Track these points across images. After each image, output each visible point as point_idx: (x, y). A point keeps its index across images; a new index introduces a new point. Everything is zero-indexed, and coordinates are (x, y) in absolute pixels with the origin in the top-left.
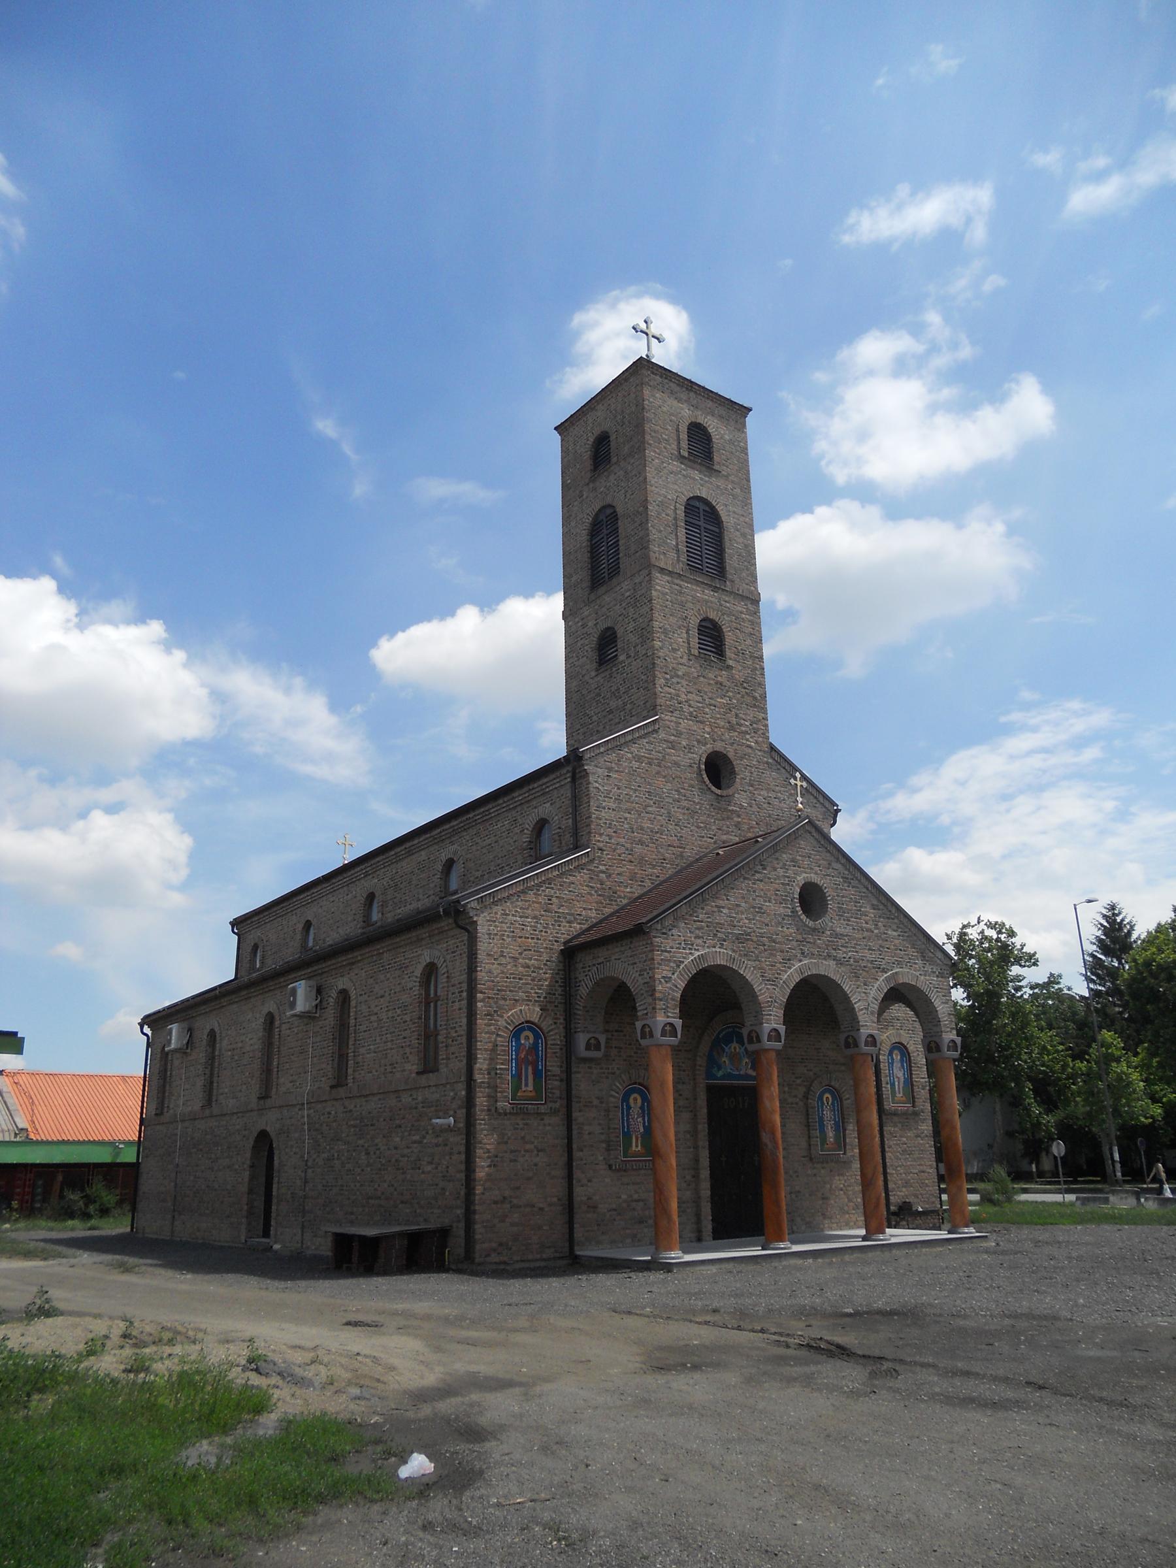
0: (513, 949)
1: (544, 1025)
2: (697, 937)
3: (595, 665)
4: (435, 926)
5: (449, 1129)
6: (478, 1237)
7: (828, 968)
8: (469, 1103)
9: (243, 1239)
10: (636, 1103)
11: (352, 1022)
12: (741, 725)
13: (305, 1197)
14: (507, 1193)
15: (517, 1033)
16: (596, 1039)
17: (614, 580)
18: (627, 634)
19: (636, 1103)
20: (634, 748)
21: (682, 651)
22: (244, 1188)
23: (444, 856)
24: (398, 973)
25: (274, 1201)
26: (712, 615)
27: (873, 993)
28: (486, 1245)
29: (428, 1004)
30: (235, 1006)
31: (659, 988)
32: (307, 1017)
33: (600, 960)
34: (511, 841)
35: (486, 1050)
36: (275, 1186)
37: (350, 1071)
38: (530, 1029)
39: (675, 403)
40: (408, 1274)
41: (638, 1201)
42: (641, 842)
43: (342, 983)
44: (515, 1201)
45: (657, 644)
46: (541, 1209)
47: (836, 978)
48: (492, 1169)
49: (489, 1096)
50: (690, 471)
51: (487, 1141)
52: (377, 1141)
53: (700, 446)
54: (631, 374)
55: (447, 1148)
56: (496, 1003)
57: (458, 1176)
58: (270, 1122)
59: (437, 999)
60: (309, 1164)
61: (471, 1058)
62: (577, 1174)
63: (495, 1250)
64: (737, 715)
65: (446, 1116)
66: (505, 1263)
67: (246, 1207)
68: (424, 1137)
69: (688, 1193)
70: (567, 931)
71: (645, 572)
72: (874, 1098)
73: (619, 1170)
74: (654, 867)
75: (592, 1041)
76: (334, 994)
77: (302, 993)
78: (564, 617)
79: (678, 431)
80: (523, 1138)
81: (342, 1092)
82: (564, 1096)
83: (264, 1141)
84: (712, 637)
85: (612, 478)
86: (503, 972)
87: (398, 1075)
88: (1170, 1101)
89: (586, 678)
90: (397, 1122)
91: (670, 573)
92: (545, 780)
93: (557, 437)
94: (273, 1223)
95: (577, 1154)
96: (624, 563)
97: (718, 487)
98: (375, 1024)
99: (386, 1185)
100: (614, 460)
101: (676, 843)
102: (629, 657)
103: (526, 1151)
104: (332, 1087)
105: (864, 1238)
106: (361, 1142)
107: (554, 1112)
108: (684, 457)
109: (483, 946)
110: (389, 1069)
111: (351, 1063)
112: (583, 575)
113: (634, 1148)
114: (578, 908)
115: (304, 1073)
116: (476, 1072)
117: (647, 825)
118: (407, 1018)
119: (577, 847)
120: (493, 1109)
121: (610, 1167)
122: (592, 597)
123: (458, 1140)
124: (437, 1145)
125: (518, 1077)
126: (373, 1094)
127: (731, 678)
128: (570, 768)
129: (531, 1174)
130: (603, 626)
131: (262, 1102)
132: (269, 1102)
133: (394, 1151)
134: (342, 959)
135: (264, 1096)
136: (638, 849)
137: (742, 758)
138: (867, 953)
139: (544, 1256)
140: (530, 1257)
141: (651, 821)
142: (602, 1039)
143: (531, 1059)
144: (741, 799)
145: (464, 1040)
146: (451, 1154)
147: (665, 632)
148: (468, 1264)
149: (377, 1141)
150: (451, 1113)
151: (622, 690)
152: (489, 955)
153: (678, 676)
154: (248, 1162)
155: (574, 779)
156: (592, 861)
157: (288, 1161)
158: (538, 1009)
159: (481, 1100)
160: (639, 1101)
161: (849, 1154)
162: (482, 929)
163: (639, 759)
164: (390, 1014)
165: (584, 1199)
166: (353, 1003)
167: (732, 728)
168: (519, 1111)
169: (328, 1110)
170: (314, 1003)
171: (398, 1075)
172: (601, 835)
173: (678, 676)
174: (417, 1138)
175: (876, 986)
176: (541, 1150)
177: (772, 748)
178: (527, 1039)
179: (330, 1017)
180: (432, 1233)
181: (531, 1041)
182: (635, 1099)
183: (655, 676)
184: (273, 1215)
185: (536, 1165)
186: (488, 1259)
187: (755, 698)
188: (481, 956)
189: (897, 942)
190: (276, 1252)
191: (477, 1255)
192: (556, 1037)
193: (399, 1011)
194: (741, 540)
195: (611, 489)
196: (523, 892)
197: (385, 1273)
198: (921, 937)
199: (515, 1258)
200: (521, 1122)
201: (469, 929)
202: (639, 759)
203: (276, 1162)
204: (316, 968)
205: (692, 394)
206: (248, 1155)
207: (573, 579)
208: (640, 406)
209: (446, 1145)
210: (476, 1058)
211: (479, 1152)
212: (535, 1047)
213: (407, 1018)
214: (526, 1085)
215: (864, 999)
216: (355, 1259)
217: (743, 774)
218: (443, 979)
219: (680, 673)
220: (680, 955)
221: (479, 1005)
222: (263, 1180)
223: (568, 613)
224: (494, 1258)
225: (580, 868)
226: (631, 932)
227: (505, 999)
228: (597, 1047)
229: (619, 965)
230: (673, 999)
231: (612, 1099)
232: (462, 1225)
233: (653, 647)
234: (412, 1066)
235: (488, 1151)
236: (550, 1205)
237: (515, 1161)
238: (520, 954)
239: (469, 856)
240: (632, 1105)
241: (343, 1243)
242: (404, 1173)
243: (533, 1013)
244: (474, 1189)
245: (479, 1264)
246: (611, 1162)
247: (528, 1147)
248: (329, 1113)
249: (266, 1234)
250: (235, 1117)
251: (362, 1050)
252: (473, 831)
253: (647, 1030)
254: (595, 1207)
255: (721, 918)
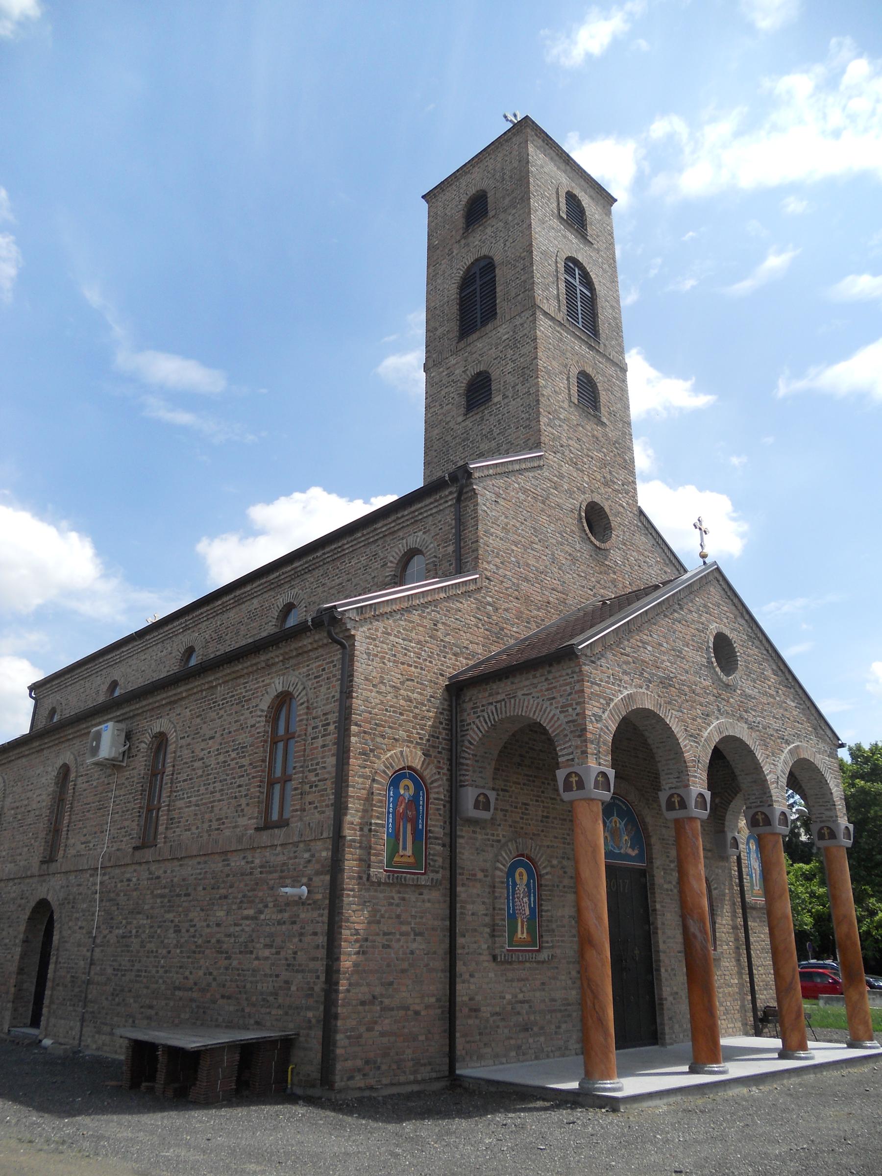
0: (395, 676)
1: (427, 774)
2: (625, 673)
3: (462, 410)
4: (294, 645)
5: (300, 902)
6: (339, 1051)
7: (741, 731)
8: (335, 866)
9: (6, 1028)
10: (521, 879)
11: (169, 770)
12: (614, 483)
13: (89, 982)
14: (378, 990)
15: (395, 782)
16: (486, 796)
17: (490, 326)
18: (503, 376)
19: (521, 879)
20: (521, 479)
21: (564, 396)
22: (13, 967)
23: (281, 600)
24: (236, 708)
25: (49, 984)
26: (589, 370)
27: (780, 766)
28: (349, 1064)
29: (274, 743)
30: (24, 760)
31: (590, 727)
32: (113, 766)
33: (499, 697)
34: (369, 578)
35: (359, 798)
36: (51, 967)
37: (161, 829)
38: (411, 778)
39: (555, 169)
40: (239, 1104)
41: (522, 1002)
42: (526, 580)
43: (159, 725)
44: (387, 1001)
45: (542, 382)
46: (417, 1013)
47: (749, 742)
48: (361, 958)
49: (360, 860)
50: (568, 234)
51: (356, 918)
52: (191, 915)
53: (575, 217)
54: (514, 135)
55: (296, 927)
56: (373, 740)
57: (312, 965)
58: (52, 890)
59: (290, 736)
60: (98, 941)
61: (340, 808)
62: (460, 967)
63: (359, 1070)
64: (610, 472)
65: (296, 883)
66: (371, 1088)
67: (12, 990)
68: (261, 912)
69: (574, 992)
70: (457, 665)
71: (527, 314)
72: (705, 891)
73: (502, 963)
74: (539, 609)
75: (481, 798)
76: (147, 738)
77: (108, 738)
78: (426, 369)
79: (557, 193)
80: (398, 917)
81: (148, 854)
82: (448, 866)
83: (43, 915)
84: (588, 394)
85: (489, 231)
86: (382, 703)
87: (227, 832)
88: (817, 911)
89: (451, 425)
90: (223, 892)
91: (552, 319)
92: (420, 505)
93: (425, 205)
94: (45, 1011)
95: (460, 941)
96: (502, 306)
97: (591, 257)
98: (200, 772)
99: (201, 973)
100: (491, 214)
101: (560, 588)
102: (505, 397)
103: (402, 934)
104: (136, 848)
105: (784, 1054)
106: (170, 916)
107: (435, 885)
108: (562, 218)
109: (361, 667)
110: (215, 825)
111: (163, 819)
112: (453, 326)
113: (519, 935)
114: (465, 638)
115: (101, 833)
116: (346, 826)
117: (532, 562)
118: (245, 762)
119: (460, 570)
120: (365, 877)
121: (494, 958)
122: (462, 345)
123: (317, 919)
124: (280, 923)
125: (395, 836)
126: (191, 857)
127: (605, 435)
128: (453, 489)
129: (405, 965)
130: (472, 371)
131: (45, 866)
132: (53, 867)
133: (215, 929)
134: (161, 697)
135: (49, 859)
136: (524, 586)
137: (616, 516)
138: (772, 721)
139: (419, 1077)
140: (402, 1079)
141: (538, 559)
142: (492, 795)
143: (410, 816)
144: (616, 556)
145: (329, 785)
146: (301, 934)
147: (548, 373)
148: (322, 1090)
149: (191, 915)
150: (305, 880)
151: (496, 431)
152: (367, 679)
153: (560, 419)
154: (21, 936)
155: (459, 500)
156: (479, 589)
157: (71, 939)
158: (420, 753)
159: (351, 864)
160: (525, 877)
161: (719, 950)
162: (361, 646)
163: (525, 491)
164: (221, 758)
165: (466, 998)
166: (171, 748)
167: (606, 484)
168: (396, 880)
169: (128, 876)
170: (122, 749)
171: (227, 832)
172: (489, 563)
173: (560, 419)
174: (251, 912)
175: (782, 758)
176: (420, 934)
177: (641, 513)
178: (407, 789)
179: (140, 765)
180: (270, 1043)
181: (412, 792)
182: (521, 874)
183: (538, 414)
184: (46, 1002)
185: (412, 953)
186: (351, 1083)
187: (625, 460)
188: (358, 679)
189: (795, 713)
190: (45, 1048)
191: (337, 1078)
192: (439, 791)
193: (233, 755)
194: (610, 311)
195: (489, 241)
196: (407, 610)
197: (208, 1102)
198: (814, 711)
199: (385, 1081)
200: (396, 896)
201: (344, 644)
202: (525, 491)
203: (56, 938)
204: (127, 709)
205: (568, 168)
206: (22, 928)
207: (439, 332)
208: (525, 161)
209: (294, 923)
210: (347, 808)
211: (345, 933)
212: (414, 801)
213: (245, 762)
214: (405, 848)
215: (775, 769)
216: (161, 1076)
217: (617, 535)
218: (300, 711)
219: (562, 417)
220: (609, 693)
221: (353, 739)
222: (36, 958)
223: (431, 364)
224: (359, 1081)
225: (467, 594)
226: (553, 657)
227: (383, 737)
228: (487, 807)
229: (531, 701)
230: (605, 744)
231: (498, 873)
232: (317, 1033)
233: (537, 384)
234: (248, 821)
235: (357, 933)
236: (427, 1007)
237: (389, 946)
238: (402, 683)
239: (313, 599)
240: (518, 881)
241: (143, 1052)
242: (228, 958)
243: (416, 759)
244: (337, 983)
245: (340, 1091)
246: (497, 951)
247: (404, 928)
248: (129, 880)
249: (35, 1022)
250: (11, 883)
251: (179, 804)
252: (317, 573)
253: (574, 779)
254: (477, 1010)
255: (646, 654)
